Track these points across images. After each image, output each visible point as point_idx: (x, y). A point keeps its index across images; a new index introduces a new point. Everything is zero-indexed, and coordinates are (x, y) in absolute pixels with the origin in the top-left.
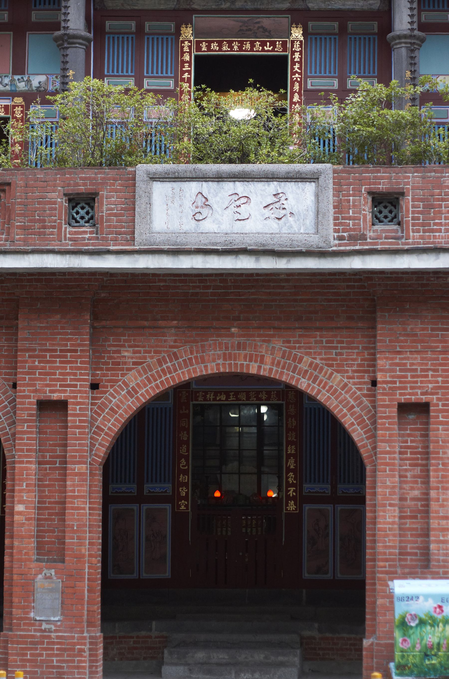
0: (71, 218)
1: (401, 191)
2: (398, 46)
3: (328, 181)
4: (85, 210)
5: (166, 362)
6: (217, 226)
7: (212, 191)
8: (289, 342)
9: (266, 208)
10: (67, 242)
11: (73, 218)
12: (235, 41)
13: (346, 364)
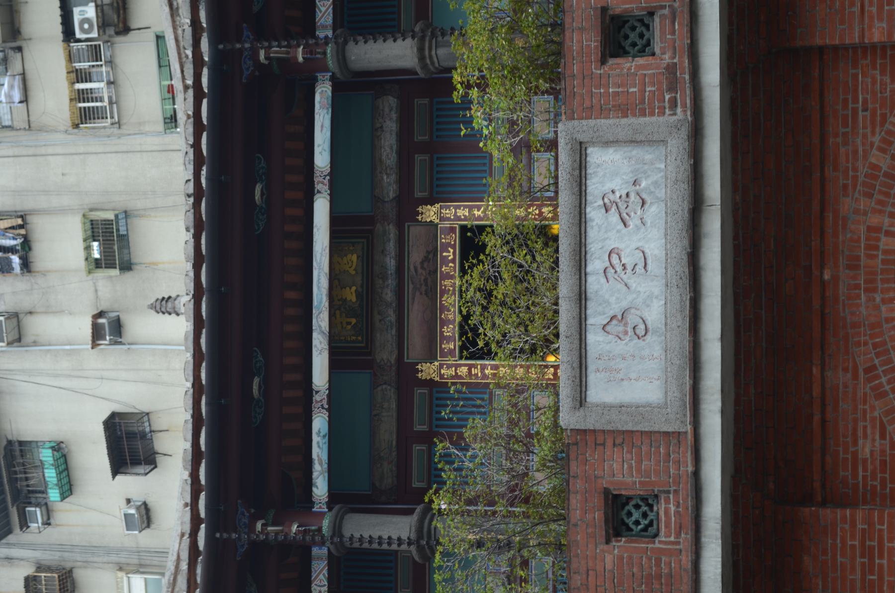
0: (645, 534)
1: (599, 12)
2: (435, 59)
3: (583, 128)
4: (633, 511)
5: (881, 385)
6: (655, 300)
7: (600, 309)
8: (845, 187)
9: (627, 224)
10: (681, 540)
11: (645, 529)
12: (441, 301)
13: (881, 93)
